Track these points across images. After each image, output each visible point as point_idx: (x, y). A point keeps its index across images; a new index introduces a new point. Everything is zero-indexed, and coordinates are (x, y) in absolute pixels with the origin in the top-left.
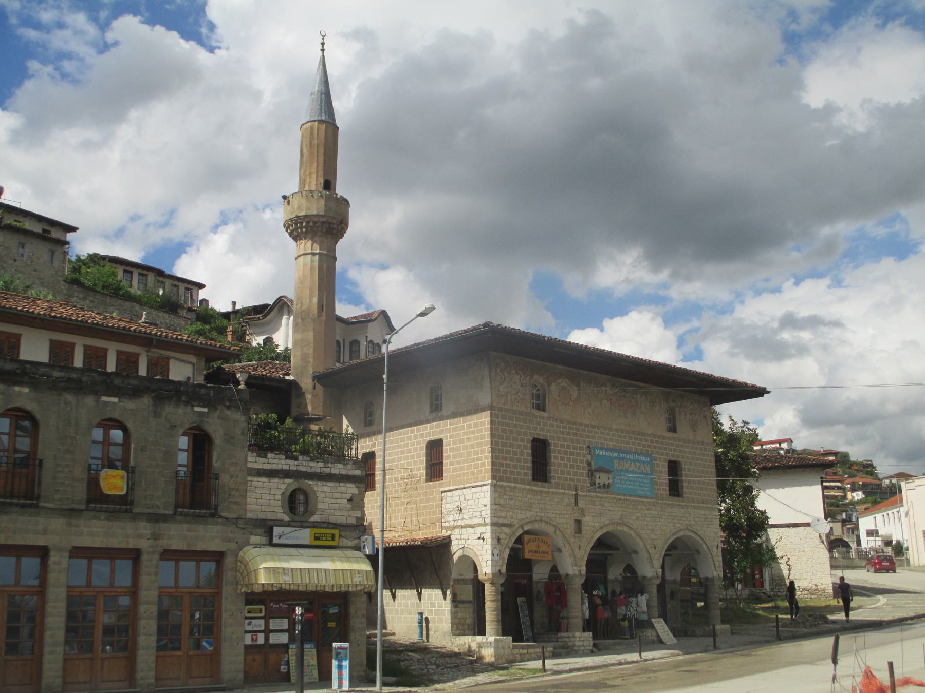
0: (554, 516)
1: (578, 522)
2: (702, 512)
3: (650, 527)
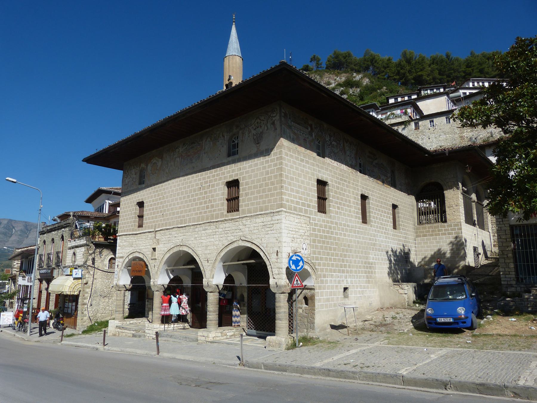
0: (142, 247)
1: (154, 249)
2: (258, 220)
3: (204, 244)
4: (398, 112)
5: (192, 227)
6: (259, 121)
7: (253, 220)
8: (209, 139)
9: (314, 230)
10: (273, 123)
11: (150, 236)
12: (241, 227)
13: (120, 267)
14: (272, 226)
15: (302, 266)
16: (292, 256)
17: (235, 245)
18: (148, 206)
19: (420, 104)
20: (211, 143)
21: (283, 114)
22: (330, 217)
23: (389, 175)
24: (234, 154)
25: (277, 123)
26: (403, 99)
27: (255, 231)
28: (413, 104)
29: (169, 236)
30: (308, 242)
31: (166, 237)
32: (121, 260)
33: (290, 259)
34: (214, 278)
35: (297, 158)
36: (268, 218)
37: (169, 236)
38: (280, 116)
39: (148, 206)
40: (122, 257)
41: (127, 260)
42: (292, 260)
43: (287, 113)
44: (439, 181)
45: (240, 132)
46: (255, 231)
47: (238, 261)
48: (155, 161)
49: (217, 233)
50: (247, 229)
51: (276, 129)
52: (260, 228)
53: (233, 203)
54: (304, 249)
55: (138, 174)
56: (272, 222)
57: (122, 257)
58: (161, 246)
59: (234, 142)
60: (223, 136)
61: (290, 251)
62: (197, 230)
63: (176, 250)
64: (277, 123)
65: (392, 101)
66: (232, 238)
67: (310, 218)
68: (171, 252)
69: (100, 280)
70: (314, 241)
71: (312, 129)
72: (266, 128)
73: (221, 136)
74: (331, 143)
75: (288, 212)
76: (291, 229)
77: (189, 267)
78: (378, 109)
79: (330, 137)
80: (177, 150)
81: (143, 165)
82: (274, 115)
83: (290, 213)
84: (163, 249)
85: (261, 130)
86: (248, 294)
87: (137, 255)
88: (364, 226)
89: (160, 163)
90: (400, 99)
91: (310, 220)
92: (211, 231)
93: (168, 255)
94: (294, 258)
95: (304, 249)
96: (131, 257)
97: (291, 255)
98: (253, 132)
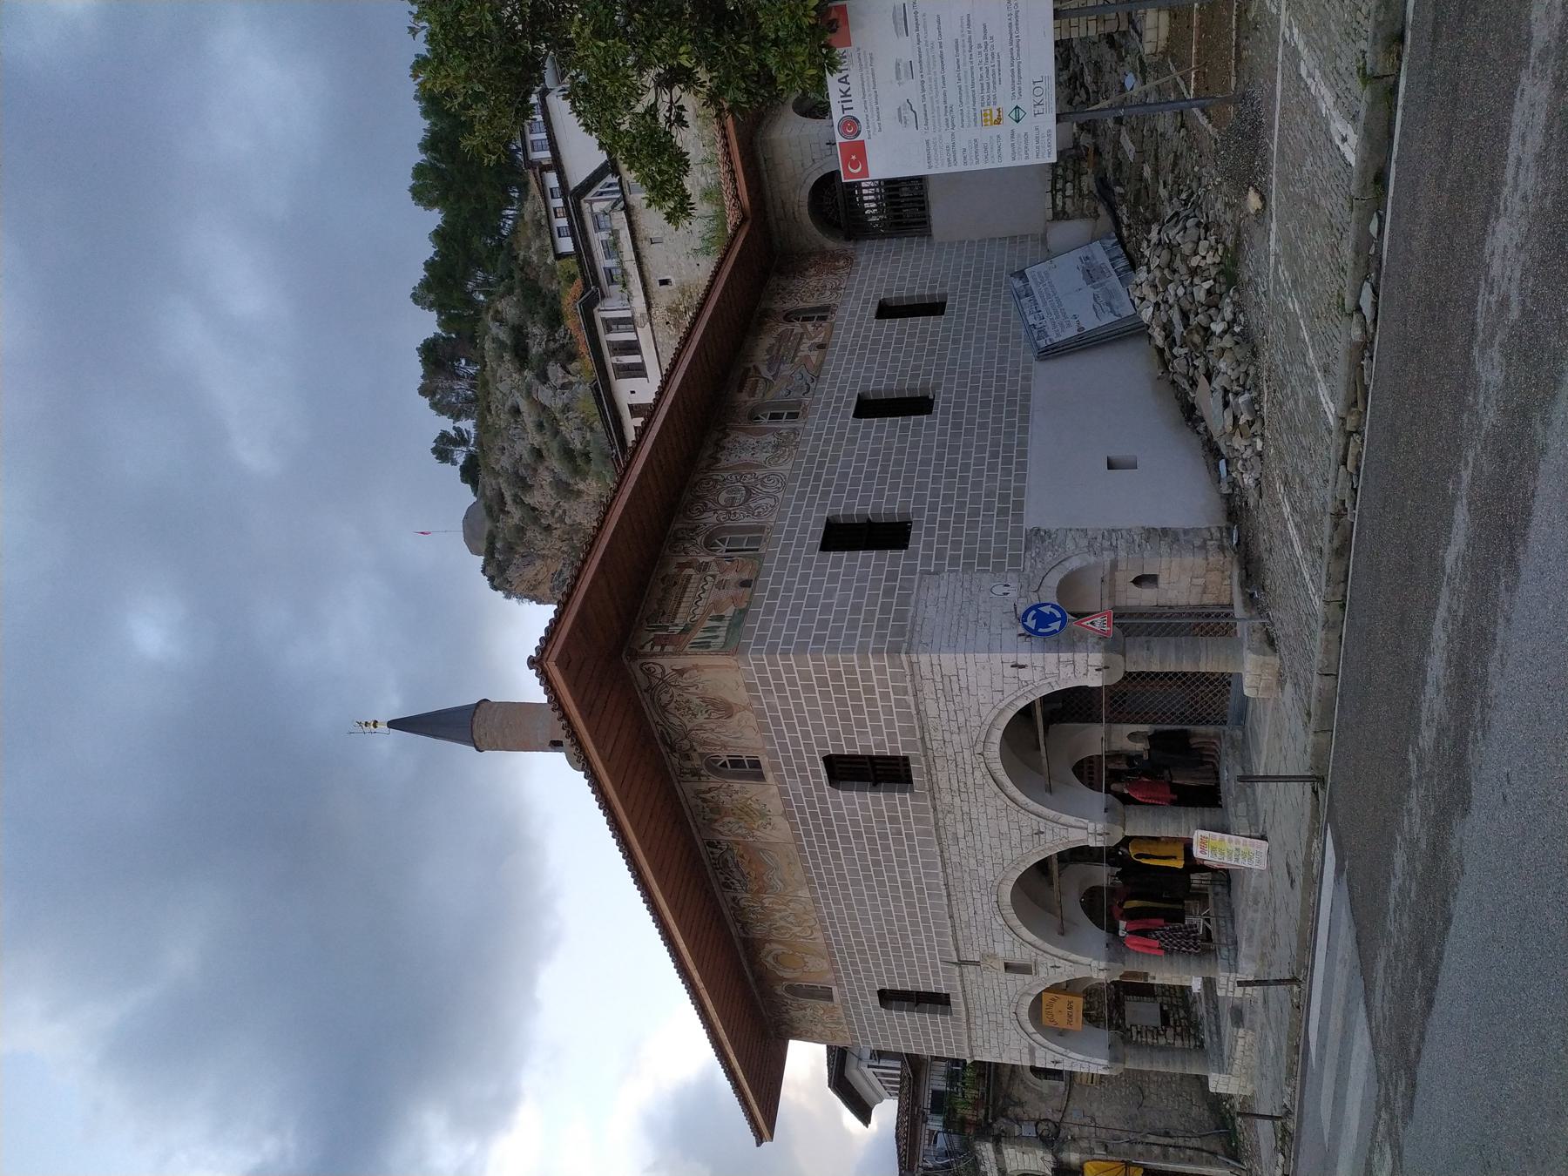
4: (597, 239)
5: (949, 871)
6: (673, 705)
7: (932, 723)
8: (716, 826)
9: (954, 561)
10: (681, 672)
11: (973, 977)
12: (950, 752)
13: (1058, 1058)
14: (946, 680)
15: (1053, 606)
16: (1026, 627)
17: (998, 768)
18: (891, 979)
19: (576, 178)
20: (727, 819)
21: (657, 649)
22: (919, 512)
23: (797, 327)
24: (756, 764)
25: (680, 662)
26: (560, 212)
27: (961, 720)
28: (575, 197)
29: (973, 930)
30: (986, 577)
31: (974, 937)
32: (1039, 1053)
33: (1034, 632)
34: (1085, 824)
35: (770, 610)
36: (928, 688)
37: (973, 930)
38: (662, 654)
39: (891, 979)
40: (1032, 1051)
41: (1039, 1037)
42: (1037, 627)
43: (652, 635)
44: (812, 181)
45: (700, 750)
46: (961, 720)
47: (1038, 748)
48: (770, 959)
49: (966, 809)
50: (955, 737)
51: (696, 667)
52: (951, 707)
53: (888, 772)
54: (1006, 590)
55: (802, 1001)
56: (938, 679)
57: (1032, 1051)
58: (999, 949)
59: (724, 765)
60: (710, 790)
61: (1015, 632)
62: (955, 859)
63: (1010, 912)
64: (680, 662)
65: (566, 245)
66: (978, 774)
67: (923, 573)
68: (1016, 922)
69: (1095, 1105)
70: (984, 560)
71: (689, 565)
72: (692, 690)
73: (708, 796)
74: (724, 508)
75: (911, 638)
76: (955, 629)
77: (1056, 874)
78: (594, 294)
79: (706, 509)
80: (742, 903)
81: (780, 990)
82: (659, 670)
83: (912, 631)
84: (1008, 946)
85: (697, 701)
86: (1128, 722)
87: (1025, 1017)
88: (939, 405)
89: (775, 946)
90: (563, 222)
91: (929, 573)
92: (960, 826)
93: (1025, 933)
94: (1031, 623)
95: (1006, 590)
96: (1031, 1029)
97: (1022, 630)
98: (701, 718)
